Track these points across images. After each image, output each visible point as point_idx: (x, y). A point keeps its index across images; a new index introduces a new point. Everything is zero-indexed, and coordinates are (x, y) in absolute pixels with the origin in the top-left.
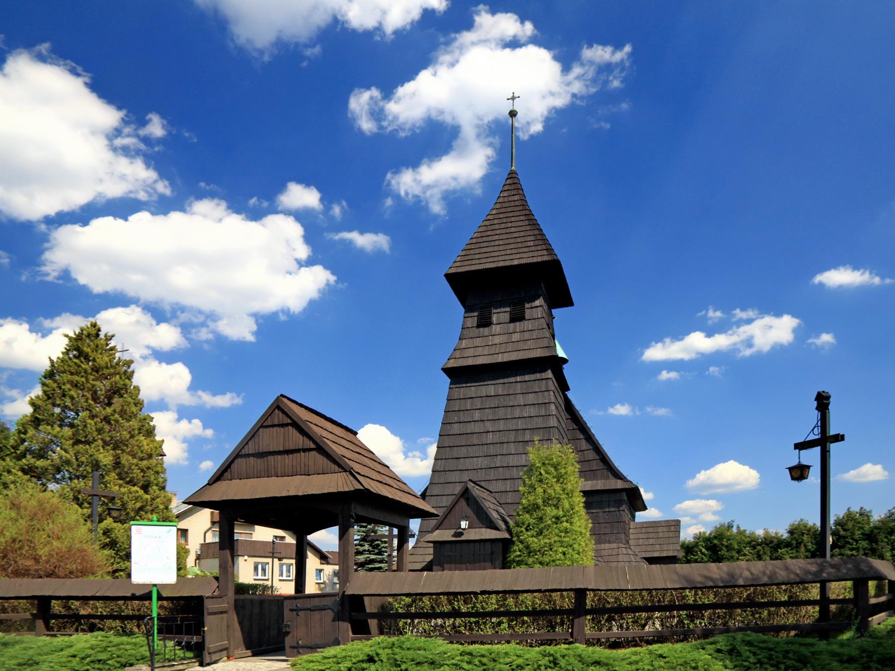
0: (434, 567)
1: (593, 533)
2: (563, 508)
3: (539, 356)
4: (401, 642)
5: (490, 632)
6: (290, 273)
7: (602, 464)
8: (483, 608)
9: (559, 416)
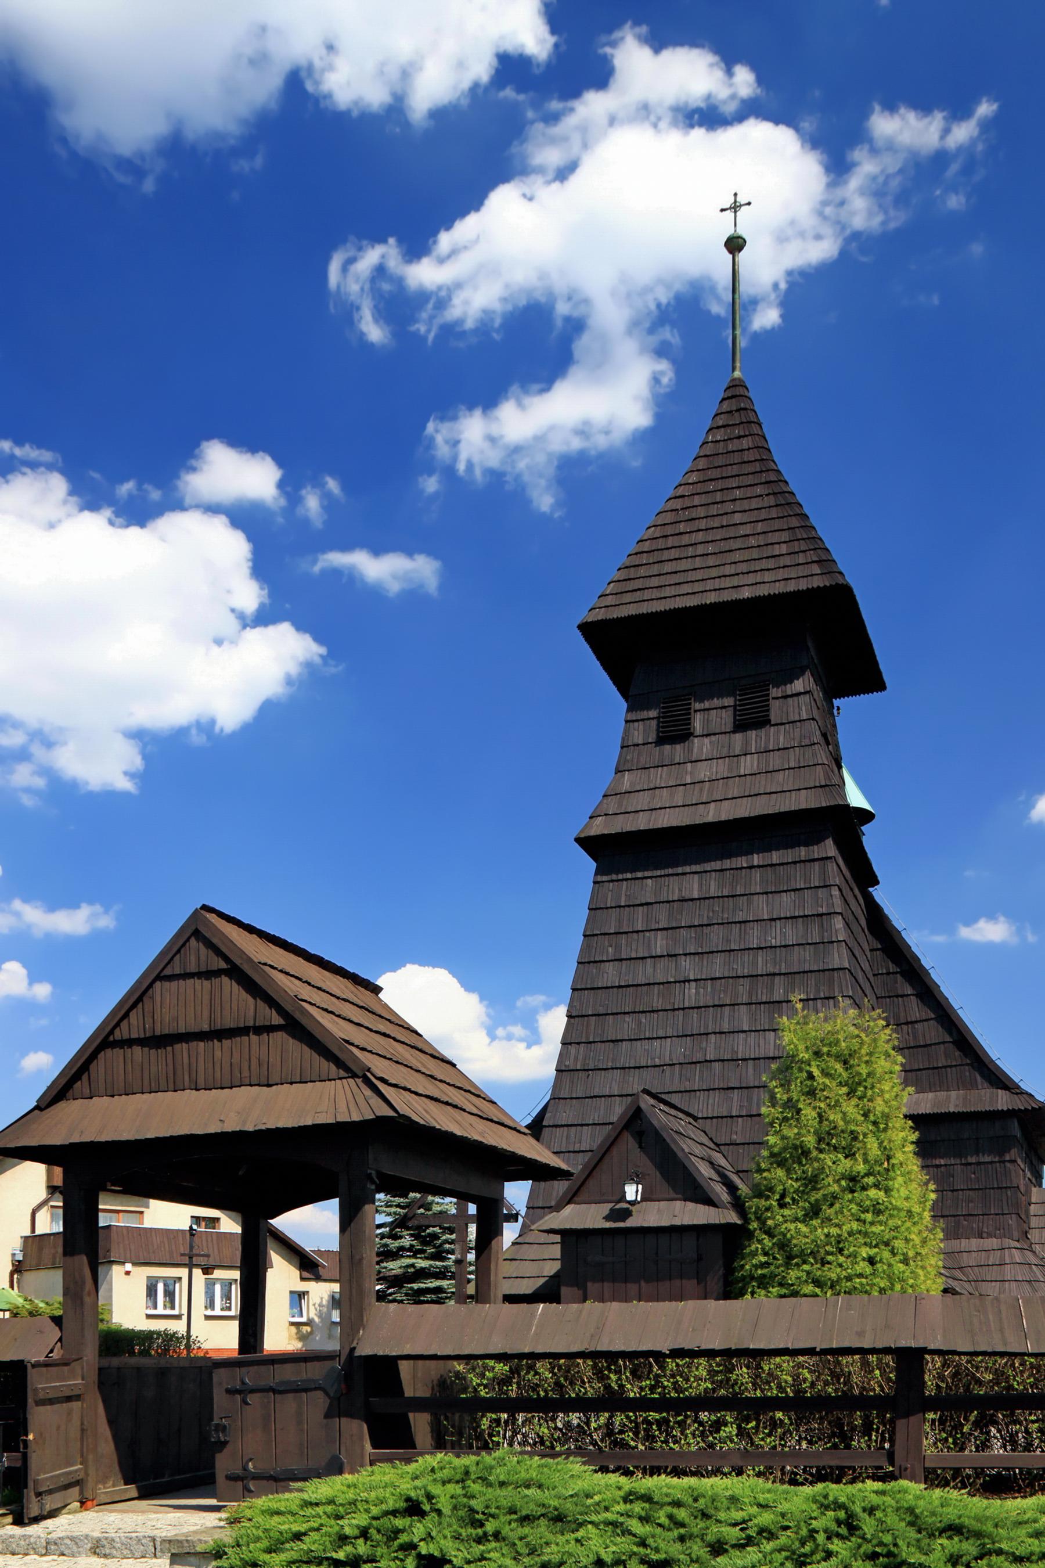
0: (565, 1291)
1: (939, 1213)
2: (865, 1154)
3: (803, 806)
4: (485, 1468)
5: (694, 1444)
6: (219, 642)
7: (957, 1053)
8: (676, 1387)
9: (852, 943)
